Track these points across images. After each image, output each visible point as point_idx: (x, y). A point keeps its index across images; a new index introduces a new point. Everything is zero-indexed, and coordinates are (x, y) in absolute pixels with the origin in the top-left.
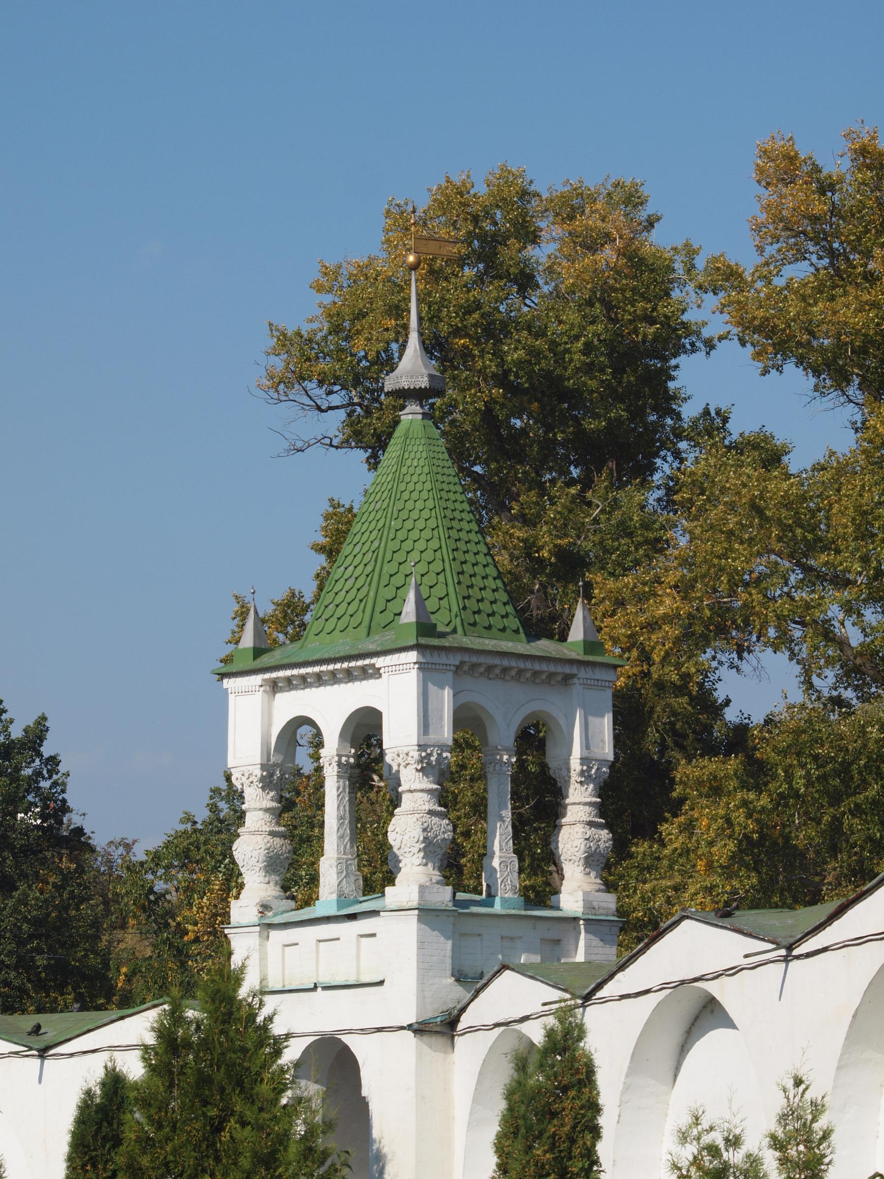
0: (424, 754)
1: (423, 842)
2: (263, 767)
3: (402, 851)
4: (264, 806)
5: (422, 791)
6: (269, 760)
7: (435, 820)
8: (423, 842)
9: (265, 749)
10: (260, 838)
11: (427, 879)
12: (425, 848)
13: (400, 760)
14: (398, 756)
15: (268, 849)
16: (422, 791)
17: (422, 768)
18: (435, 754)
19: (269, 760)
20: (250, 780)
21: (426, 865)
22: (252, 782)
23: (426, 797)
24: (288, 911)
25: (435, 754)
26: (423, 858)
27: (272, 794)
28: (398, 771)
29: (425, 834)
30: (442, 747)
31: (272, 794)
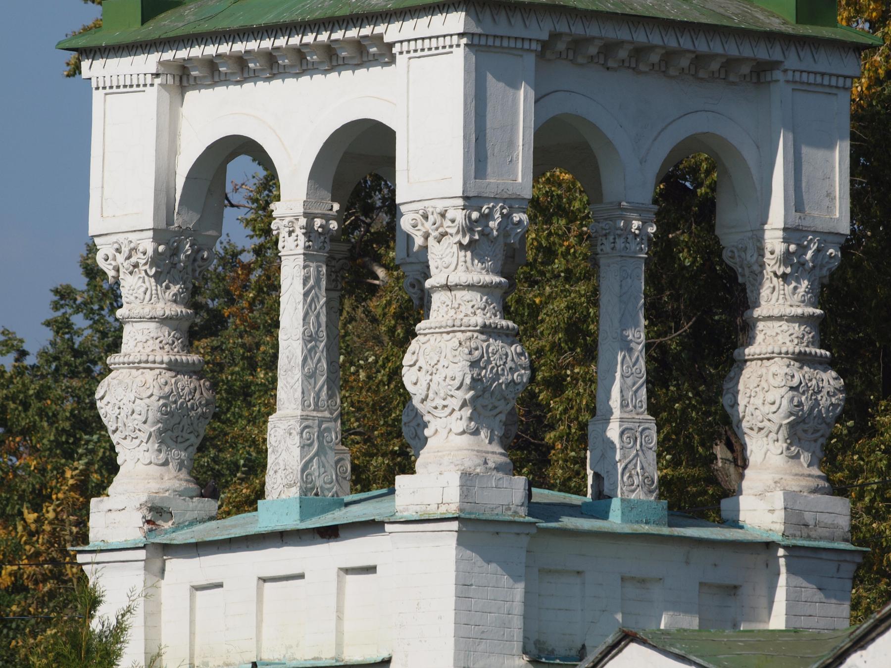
0: (475, 215)
1: (471, 388)
2: (159, 235)
3: (429, 405)
4: (159, 313)
5: (470, 287)
6: (170, 222)
7: (496, 345)
8: (471, 388)
9: (164, 201)
10: (149, 375)
11: (481, 461)
12: (474, 399)
14: (426, 217)
15: (166, 397)
16: (470, 287)
18: (497, 215)
19: (170, 222)
20: (133, 260)
21: (476, 432)
22: (136, 266)
23: (476, 298)
24: (203, 521)
25: (497, 215)
26: (471, 419)
27: (175, 289)
29: (476, 372)
31: (175, 289)
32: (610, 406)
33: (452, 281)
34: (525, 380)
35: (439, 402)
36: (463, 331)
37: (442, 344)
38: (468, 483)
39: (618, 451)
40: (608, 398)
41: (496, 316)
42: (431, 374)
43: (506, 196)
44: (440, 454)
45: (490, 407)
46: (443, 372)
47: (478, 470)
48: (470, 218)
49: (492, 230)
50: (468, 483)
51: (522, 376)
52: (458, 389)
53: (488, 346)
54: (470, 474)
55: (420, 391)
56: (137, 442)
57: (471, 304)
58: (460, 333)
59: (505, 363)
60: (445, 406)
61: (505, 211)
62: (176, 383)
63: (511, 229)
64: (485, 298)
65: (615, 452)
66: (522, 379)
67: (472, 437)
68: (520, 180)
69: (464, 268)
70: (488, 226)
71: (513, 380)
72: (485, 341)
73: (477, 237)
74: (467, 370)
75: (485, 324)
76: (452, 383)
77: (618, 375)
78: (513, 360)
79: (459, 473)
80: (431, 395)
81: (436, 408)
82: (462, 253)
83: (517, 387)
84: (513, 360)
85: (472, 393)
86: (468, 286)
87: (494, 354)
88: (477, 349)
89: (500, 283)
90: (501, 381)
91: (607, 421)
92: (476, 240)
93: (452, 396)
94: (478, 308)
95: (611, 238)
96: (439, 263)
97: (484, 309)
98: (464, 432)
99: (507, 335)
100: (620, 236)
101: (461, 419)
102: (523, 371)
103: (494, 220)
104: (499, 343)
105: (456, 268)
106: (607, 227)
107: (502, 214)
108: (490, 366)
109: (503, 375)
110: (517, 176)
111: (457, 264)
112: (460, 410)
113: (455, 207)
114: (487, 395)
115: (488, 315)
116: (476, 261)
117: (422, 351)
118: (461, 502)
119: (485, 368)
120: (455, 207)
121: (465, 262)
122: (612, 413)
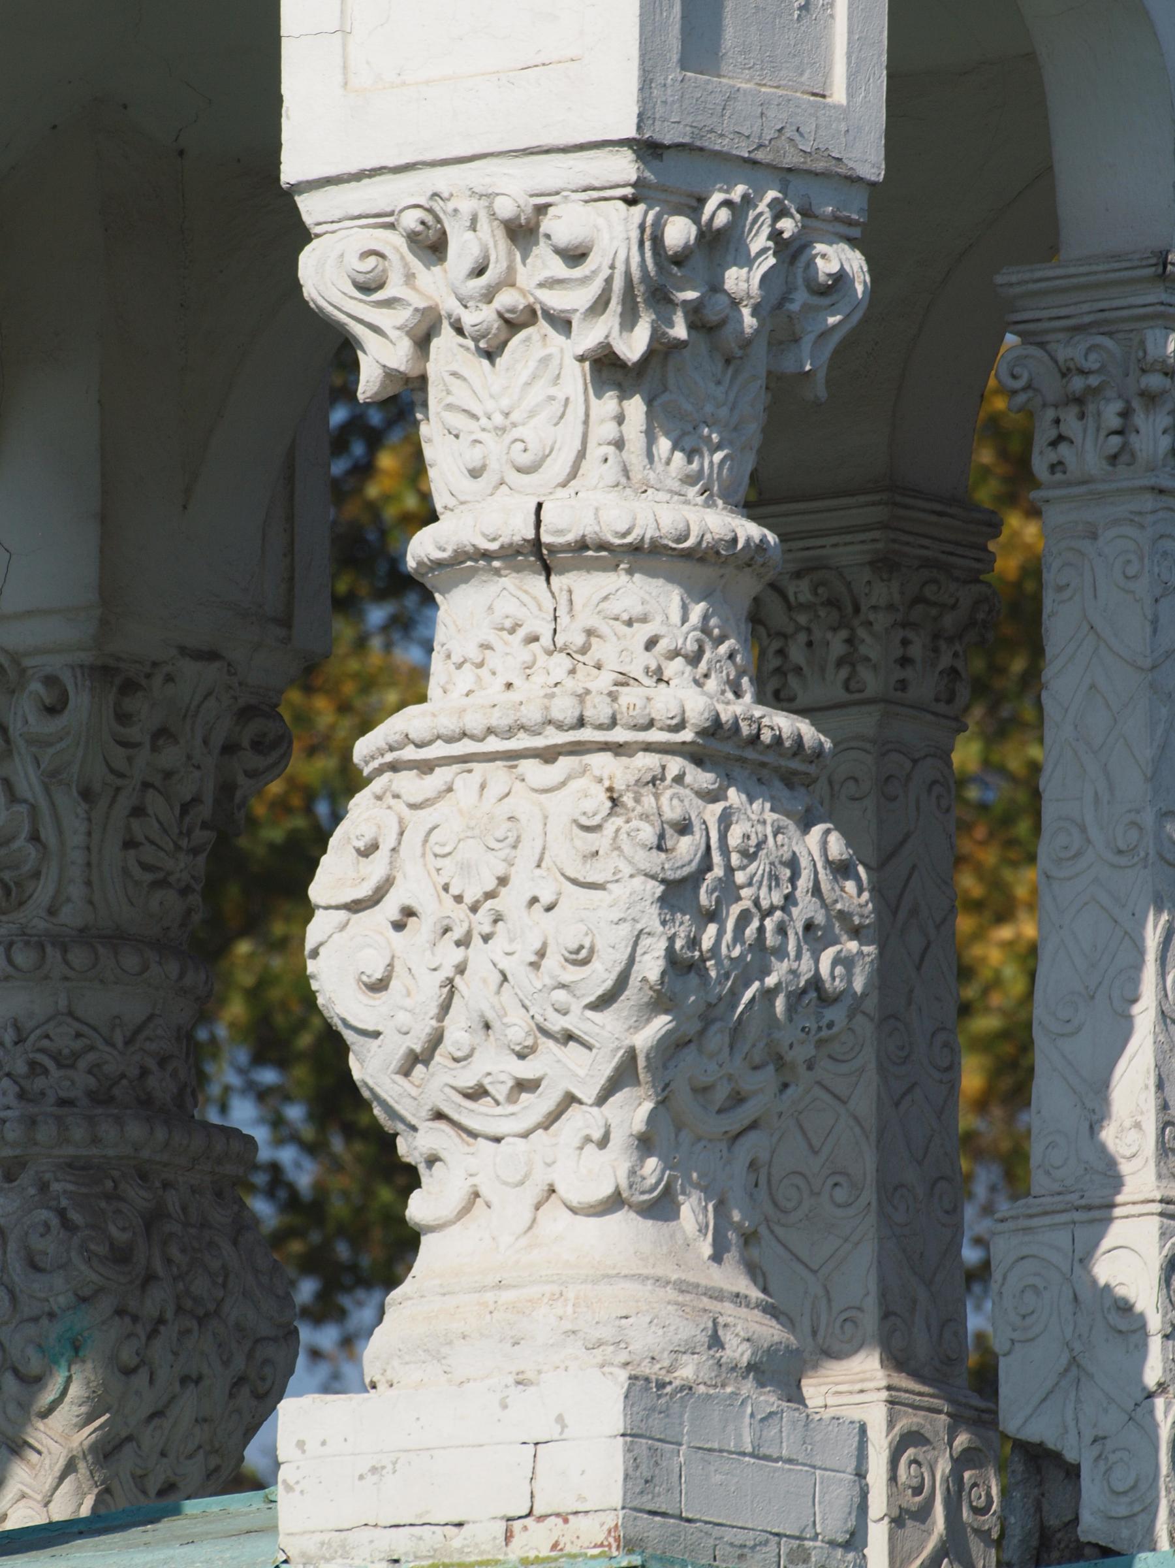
0: (679, 232)
1: (661, 1001)
3: (438, 1083)
5: (643, 555)
7: (753, 817)
8: (661, 1001)
11: (691, 1330)
12: (670, 1049)
13: (437, 286)
14: (431, 245)
16: (643, 555)
17: (661, 351)
18: (759, 241)
21: (661, 1207)
23: (665, 606)
25: (759, 241)
26: (645, 1144)
28: (406, 400)
29: (683, 927)
30: (804, 182)
32: (1102, 1149)
33: (565, 522)
34: (858, 985)
35: (496, 1066)
36: (618, 749)
37: (523, 803)
38: (656, 1424)
39: (1155, 1345)
40: (1096, 1111)
41: (738, 694)
42: (464, 942)
43: (791, 159)
44: (507, 1296)
45: (721, 1094)
46: (525, 931)
47: (687, 1371)
48: (657, 240)
49: (735, 303)
50: (656, 1422)
51: (845, 962)
52: (604, 1002)
53: (725, 821)
54: (661, 1385)
55: (403, 1018)
56: (537, 1105)
57: (643, 632)
58: (607, 757)
59: (790, 899)
60: (523, 1086)
61: (788, 226)
62: (725, 821)
63: (806, 308)
64: (698, 610)
65: (1142, 1349)
66: (849, 977)
67: (648, 1226)
68: (839, 94)
69: (611, 472)
70: (715, 286)
71: (816, 982)
72: (711, 797)
73: (680, 330)
74: (651, 917)
75: (717, 721)
76: (572, 974)
77: (1145, 1014)
78: (816, 891)
79: (623, 1375)
80: (457, 1035)
81: (477, 1093)
82: (608, 404)
83: (830, 1014)
84: (816, 891)
85: (661, 1023)
86: (636, 549)
87: (749, 856)
88: (684, 828)
89: (762, 546)
90: (771, 981)
91: (1095, 1204)
92: (679, 345)
93: (569, 1037)
94: (675, 654)
95: (1111, 415)
96: (494, 450)
97: (694, 659)
98: (615, 1202)
99: (789, 780)
100: (1151, 399)
101: (603, 1143)
102: (853, 946)
103: (748, 262)
104: (761, 809)
105: (574, 474)
106: (1092, 363)
107: (776, 235)
108: (735, 910)
109: (780, 952)
110: (827, 76)
111: (582, 455)
112: (601, 1100)
113: (594, 193)
114: (716, 1039)
115: (712, 684)
116: (664, 444)
117: (413, 838)
118: (631, 1507)
119: (713, 916)
120: (594, 193)
121: (619, 444)
122: (1116, 1182)
